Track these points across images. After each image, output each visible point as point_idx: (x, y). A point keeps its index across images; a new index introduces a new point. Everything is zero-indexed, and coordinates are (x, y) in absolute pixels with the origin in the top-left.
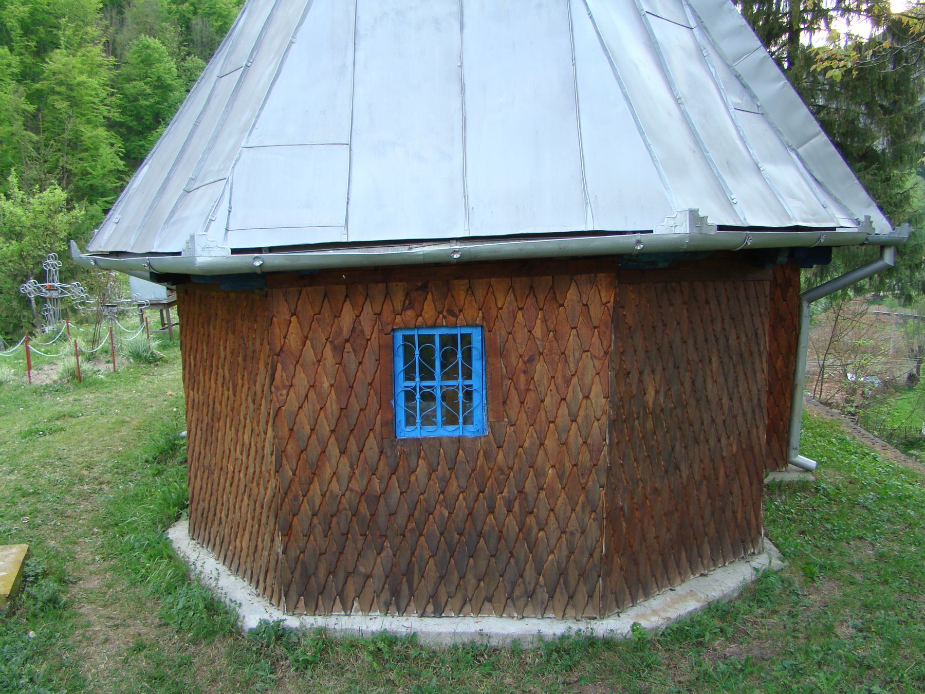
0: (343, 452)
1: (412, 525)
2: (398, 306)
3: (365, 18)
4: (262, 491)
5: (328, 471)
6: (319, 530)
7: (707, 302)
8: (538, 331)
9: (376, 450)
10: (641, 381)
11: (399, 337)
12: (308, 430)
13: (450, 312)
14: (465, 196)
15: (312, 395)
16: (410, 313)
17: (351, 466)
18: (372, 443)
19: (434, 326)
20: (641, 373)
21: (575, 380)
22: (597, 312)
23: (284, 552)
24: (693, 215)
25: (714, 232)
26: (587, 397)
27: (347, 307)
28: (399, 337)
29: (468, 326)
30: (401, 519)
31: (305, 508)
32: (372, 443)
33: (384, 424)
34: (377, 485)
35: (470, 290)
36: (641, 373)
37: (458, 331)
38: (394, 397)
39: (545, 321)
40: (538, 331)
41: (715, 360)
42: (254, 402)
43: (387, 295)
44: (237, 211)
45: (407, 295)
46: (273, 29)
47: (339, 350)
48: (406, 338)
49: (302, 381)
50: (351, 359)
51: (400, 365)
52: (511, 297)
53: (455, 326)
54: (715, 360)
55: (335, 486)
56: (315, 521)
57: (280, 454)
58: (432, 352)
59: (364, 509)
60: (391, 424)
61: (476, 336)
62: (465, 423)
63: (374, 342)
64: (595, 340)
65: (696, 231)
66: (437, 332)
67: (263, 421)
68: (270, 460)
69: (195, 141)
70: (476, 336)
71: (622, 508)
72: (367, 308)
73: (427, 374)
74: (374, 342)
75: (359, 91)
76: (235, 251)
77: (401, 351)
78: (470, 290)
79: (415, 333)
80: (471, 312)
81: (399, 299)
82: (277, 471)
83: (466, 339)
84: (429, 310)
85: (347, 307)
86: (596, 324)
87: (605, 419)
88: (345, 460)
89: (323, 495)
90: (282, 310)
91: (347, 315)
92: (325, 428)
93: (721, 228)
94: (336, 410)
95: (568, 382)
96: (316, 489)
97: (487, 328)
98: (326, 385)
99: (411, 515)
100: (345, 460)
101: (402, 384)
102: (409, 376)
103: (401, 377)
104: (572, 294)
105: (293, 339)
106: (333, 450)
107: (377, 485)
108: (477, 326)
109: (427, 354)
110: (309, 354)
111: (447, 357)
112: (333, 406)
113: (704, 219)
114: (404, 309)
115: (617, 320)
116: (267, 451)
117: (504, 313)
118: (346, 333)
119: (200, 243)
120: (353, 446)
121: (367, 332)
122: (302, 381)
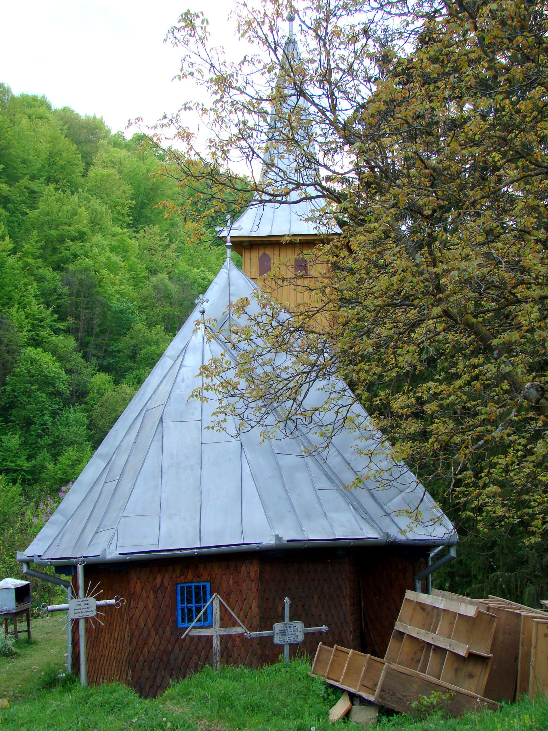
1: (184, 664)
2: (178, 575)
3: (165, 465)
4: (123, 655)
5: (151, 642)
6: (146, 668)
7: (309, 572)
8: (231, 583)
9: (170, 632)
10: (274, 603)
11: (179, 588)
12: (143, 625)
13: (198, 576)
16: (183, 577)
18: (168, 630)
19: (192, 582)
20: (274, 599)
21: (246, 602)
22: (252, 574)
23: (132, 679)
24: (277, 537)
25: (286, 542)
26: (250, 608)
28: (179, 588)
29: (205, 581)
30: (179, 661)
31: (141, 658)
32: (168, 630)
33: (173, 622)
35: (205, 568)
36: (274, 599)
37: (201, 584)
38: (177, 610)
39: (233, 579)
40: (231, 583)
41: (316, 597)
42: (121, 617)
43: (174, 570)
44: (120, 541)
45: (181, 570)
47: (156, 592)
48: (181, 587)
49: (141, 605)
50: (160, 595)
51: (179, 598)
52: (220, 570)
53: (200, 582)
54: (316, 597)
57: (132, 636)
58: (191, 592)
59: (165, 658)
60: (176, 622)
61: (208, 585)
62: (204, 621)
64: (253, 585)
65: (278, 542)
67: (125, 624)
68: (127, 639)
69: (96, 510)
70: (208, 585)
71: (268, 655)
72: (166, 576)
73: (190, 601)
75: (163, 495)
76: (120, 554)
77: (179, 592)
78: (205, 568)
79: (185, 585)
80: (206, 576)
81: (178, 572)
82: (130, 643)
83: (204, 587)
84: (190, 576)
86: (253, 578)
87: (258, 617)
88: (157, 637)
89: (149, 653)
90: (134, 577)
92: (150, 624)
93: (288, 541)
94: (154, 617)
96: (146, 650)
97: (212, 582)
98: (151, 606)
99: (184, 659)
100: (157, 637)
101: (180, 605)
102: (183, 603)
103: (179, 603)
104: (243, 568)
105: (138, 589)
106: (153, 633)
108: (208, 581)
109: (189, 593)
110: (144, 594)
111: (197, 594)
112: (153, 615)
114: (180, 575)
115: (261, 578)
117: (218, 576)
119: (108, 552)
120: (161, 631)
121: (166, 584)
122: (141, 605)
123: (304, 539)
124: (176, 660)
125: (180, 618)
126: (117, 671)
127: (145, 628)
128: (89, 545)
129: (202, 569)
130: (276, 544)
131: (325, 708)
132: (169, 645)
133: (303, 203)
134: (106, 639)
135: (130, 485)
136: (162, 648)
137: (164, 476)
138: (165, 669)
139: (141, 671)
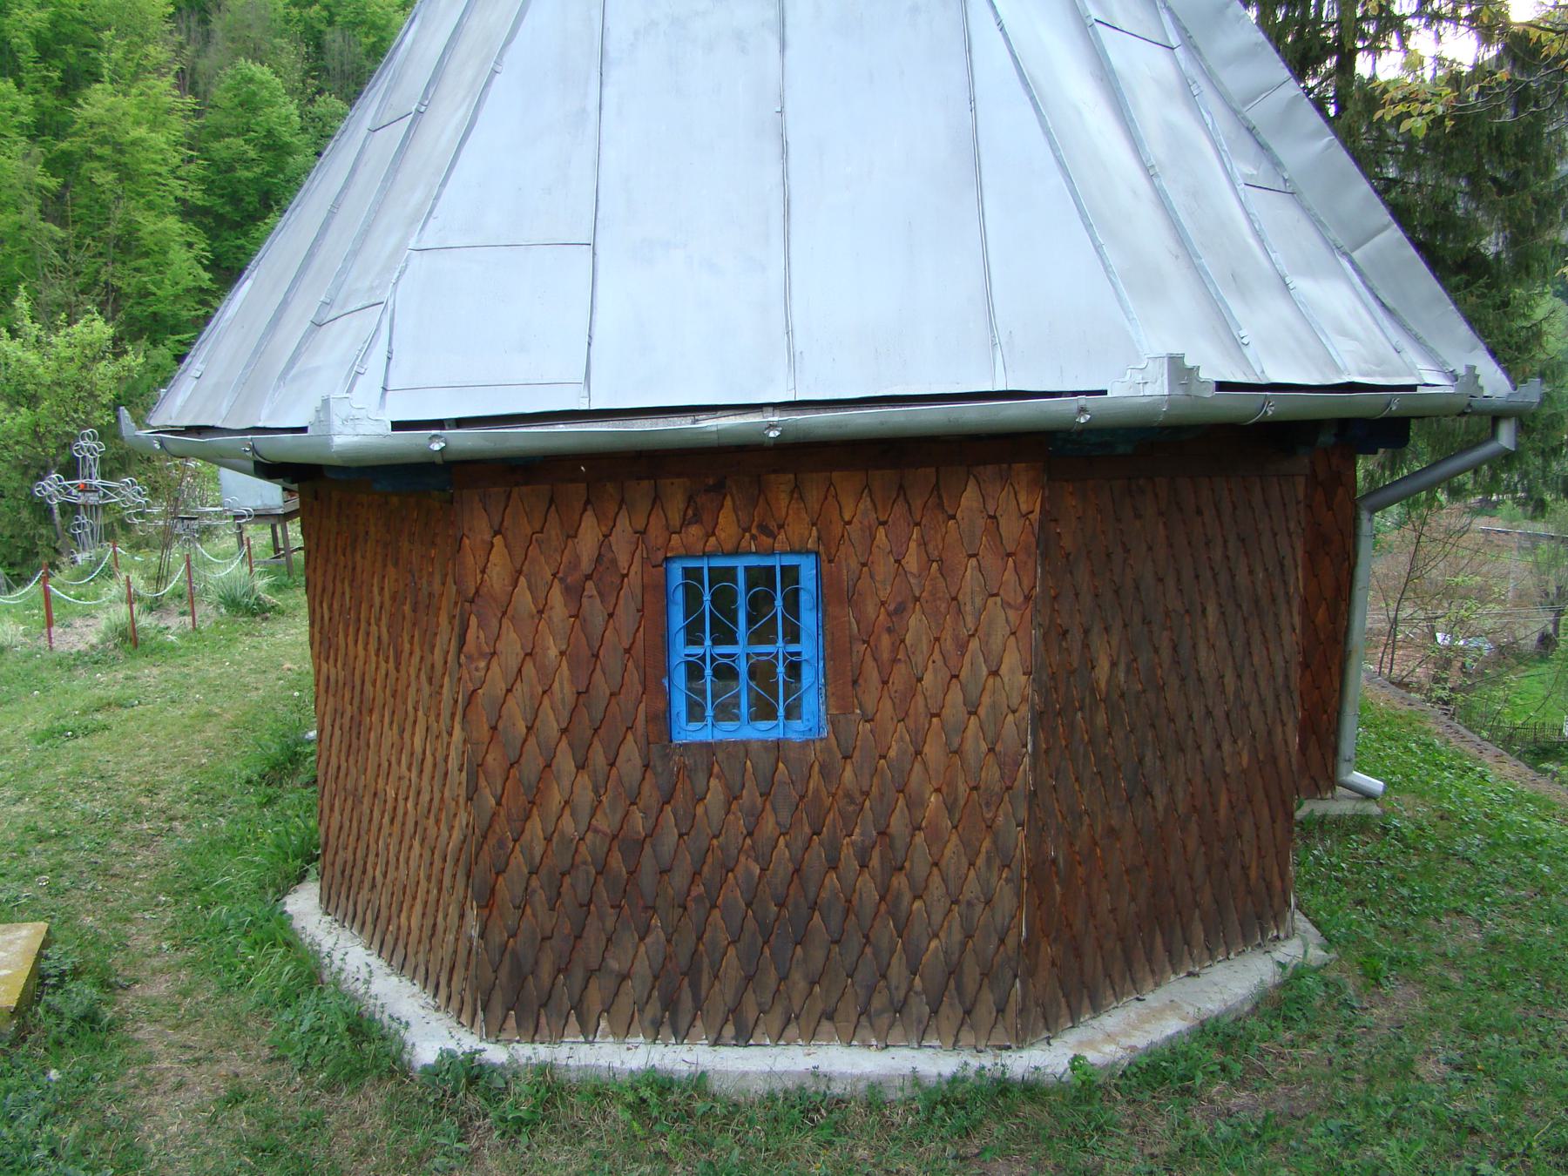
0: (581, 767)
2: (676, 520)
5: (556, 798)
6: (540, 897)
7: (1199, 512)
8: (912, 562)
10: (1086, 646)
12: (521, 727)
13: (764, 529)
14: (789, 332)
15: (529, 669)
16: (694, 530)
17: (596, 791)
19: (736, 553)
20: (1086, 632)
21: (974, 644)
22: (1011, 528)
23: (482, 936)
24: (1176, 364)
25: (1210, 393)
26: (995, 673)
27: (589, 520)
29: (793, 552)
30: (679, 879)
31: (518, 859)
32: (631, 752)
33: (652, 718)
34: (638, 822)
35: (797, 491)
36: (1086, 632)
37: (776, 562)
38: (667, 672)
39: (923, 543)
40: (912, 562)
41: (1212, 610)
42: (430, 680)
43: (656, 499)
44: (402, 358)
45: (690, 499)
46: (462, 49)
47: (574, 593)
48: (687, 572)
49: (511, 645)
50: (594, 609)
51: (678, 619)
52: (866, 503)
53: (771, 553)
54: (1212, 610)
55: (567, 824)
56: (535, 883)
57: (475, 770)
58: (732, 596)
59: (616, 862)
60: (662, 719)
61: (807, 569)
62: (788, 716)
63: (634, 579)
64: (1009, 575)
65: (1179, 391)
66: (740, 563)
67: (446, 714)
68: (458, 778)
70: (807, 569)
72: (623, 523)
73: (724, 635)
74: (634, 579)
75: (609, 154)
76: (397, 426)
77: (679, 595)
78: (797, 491)
79: (704, 564)
80: (799, 528)
81: (676, 507)
82: (469, 799)
83: (791, 574)
84: (727, 525)
85: (589, 520)
86: (1010, 548)
87: (1025, 710)
88: (584, 780)
89: (548, 840)
90: (478, 526)
91: (589, 534)
92: (551, 724)
93: (1222, 386)
94: (569, 696)
95: (962, 647)
96: (535, 827)
97: (825, 556)
98: (553, 652)
100: (584, 780)
101: (681, 651)
102: (693, 637)
103: (680, 638)
104: (970, 498)
106: (565, 762)
107: (638, 822)
109: (724, 601)
110: (524, 599)
111: (758, 605)
112: (564, 689)
113: (1193, 371)
114: (685, 523)
115: (1045, 543)
116: (453, 764)
117: (854, 530)
118: (586, 565)
119: (339, 412)
120: (598, 757)
122: (511, 645)
123: (1252, 380)
124: (663, 872)
125: (680, 705)
126: (429, 879)
127: (532, 741)
128: (283, 376)
129: (784, 499)
130: (1171, 404)
131: (1252, 1022)
132: (637, 816)
133: (570, 861)
134: (386, 744)
135: (460, 115)
136: (601, 822)
137: (614, 75)
138: (617, 907)
139: (521, 908)
